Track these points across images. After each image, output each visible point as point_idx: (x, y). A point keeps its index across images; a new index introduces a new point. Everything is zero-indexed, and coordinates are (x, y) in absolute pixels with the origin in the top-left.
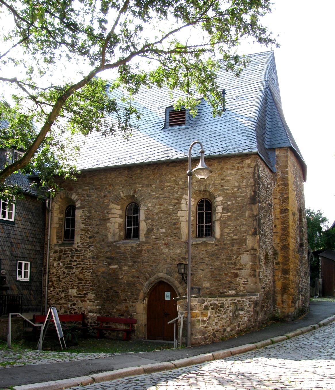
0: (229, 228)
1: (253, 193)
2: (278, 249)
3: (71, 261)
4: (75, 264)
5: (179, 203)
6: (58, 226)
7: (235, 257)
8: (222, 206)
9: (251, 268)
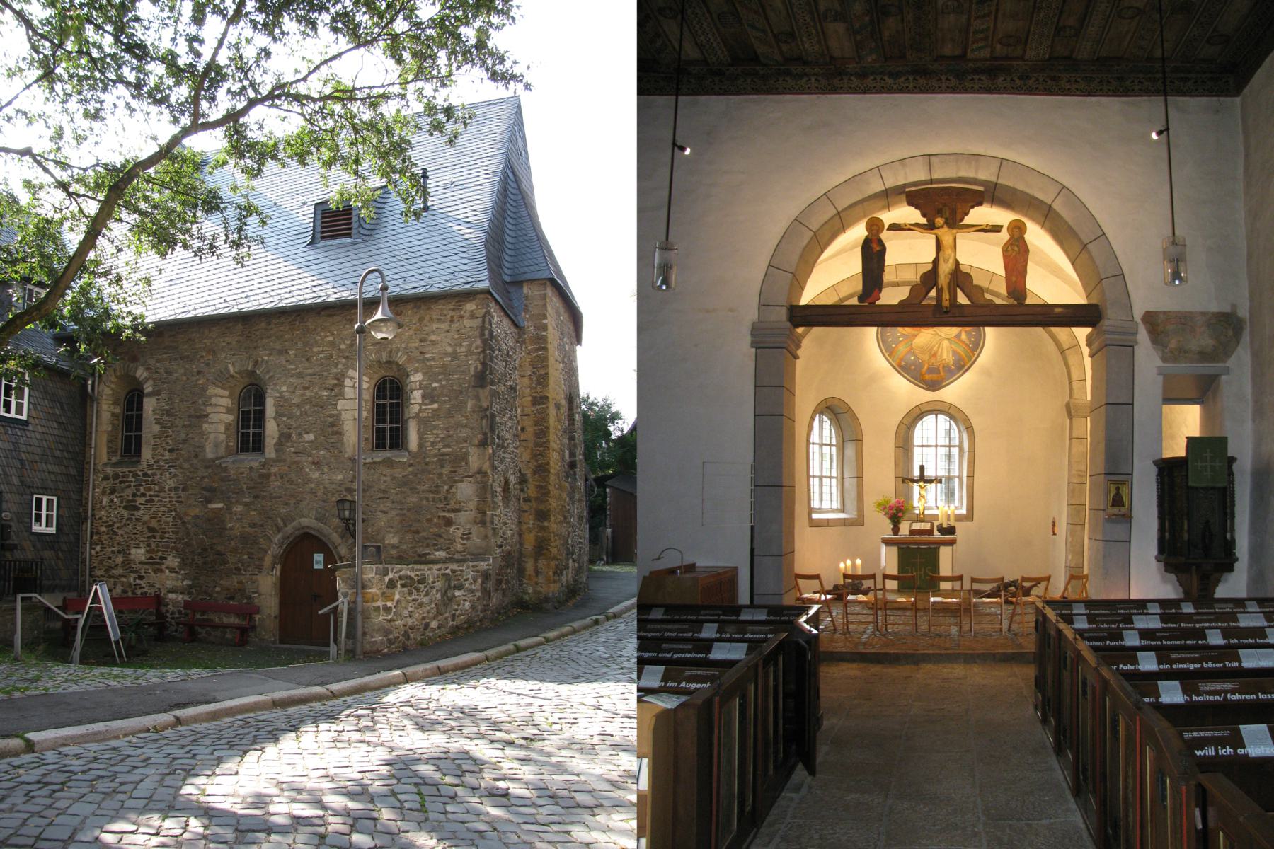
2: (529, 473)
4: (142, 500)
8: (421, 391)
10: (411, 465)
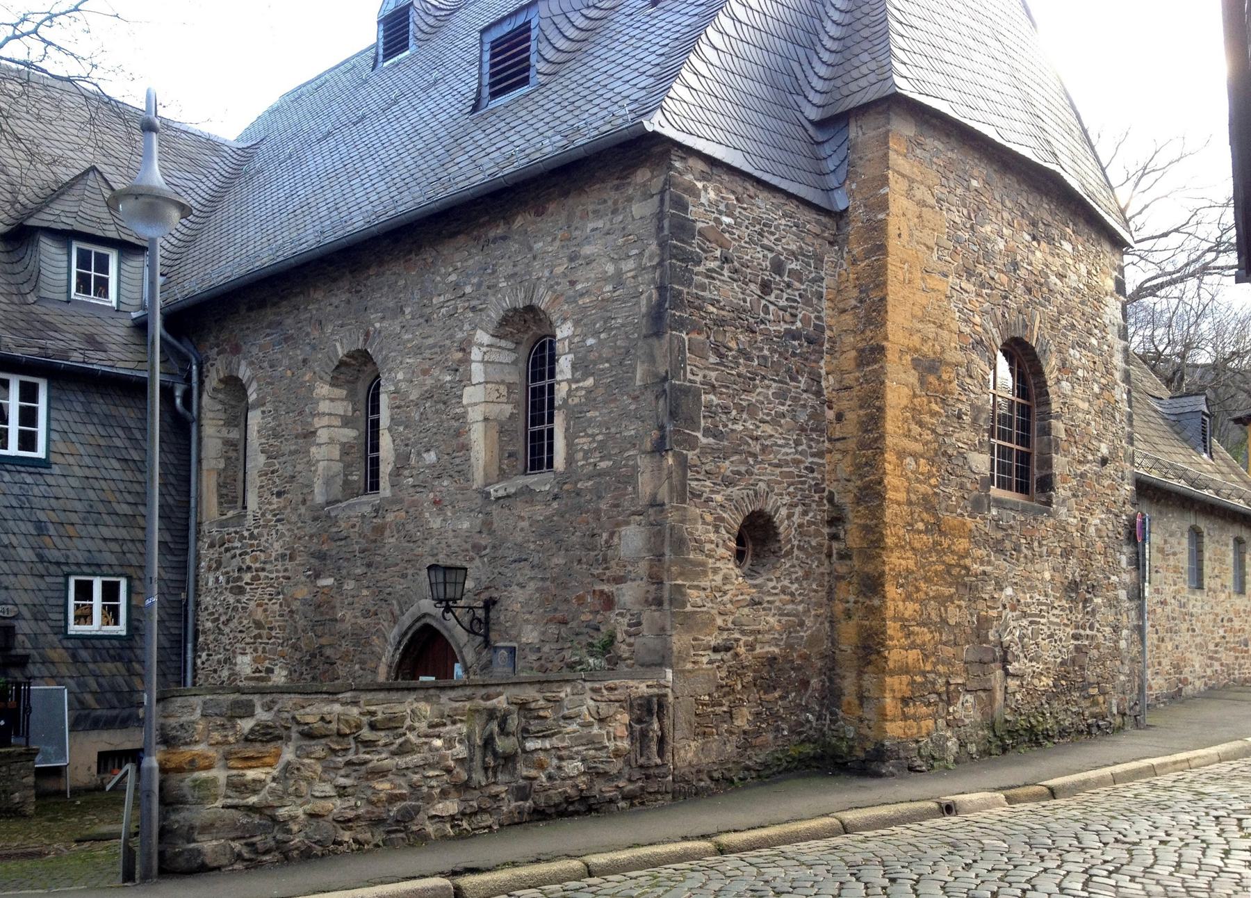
0: (590, 431)
1: (655, 296)
2: (845, 500)
3: (240, 570)
4: (247, 577)
5: (466, 361)
6: (222, 466)
7: (605, 536)
8: (571, 356)
9: (650, 576)
10: (555, 497)
